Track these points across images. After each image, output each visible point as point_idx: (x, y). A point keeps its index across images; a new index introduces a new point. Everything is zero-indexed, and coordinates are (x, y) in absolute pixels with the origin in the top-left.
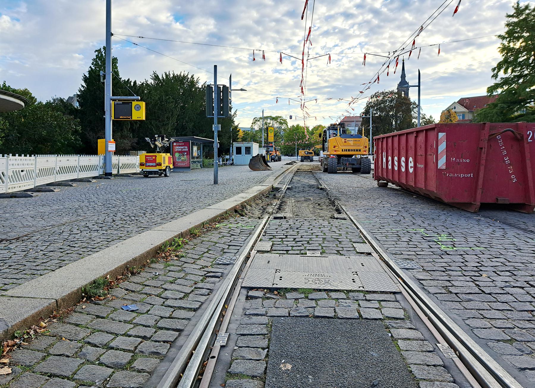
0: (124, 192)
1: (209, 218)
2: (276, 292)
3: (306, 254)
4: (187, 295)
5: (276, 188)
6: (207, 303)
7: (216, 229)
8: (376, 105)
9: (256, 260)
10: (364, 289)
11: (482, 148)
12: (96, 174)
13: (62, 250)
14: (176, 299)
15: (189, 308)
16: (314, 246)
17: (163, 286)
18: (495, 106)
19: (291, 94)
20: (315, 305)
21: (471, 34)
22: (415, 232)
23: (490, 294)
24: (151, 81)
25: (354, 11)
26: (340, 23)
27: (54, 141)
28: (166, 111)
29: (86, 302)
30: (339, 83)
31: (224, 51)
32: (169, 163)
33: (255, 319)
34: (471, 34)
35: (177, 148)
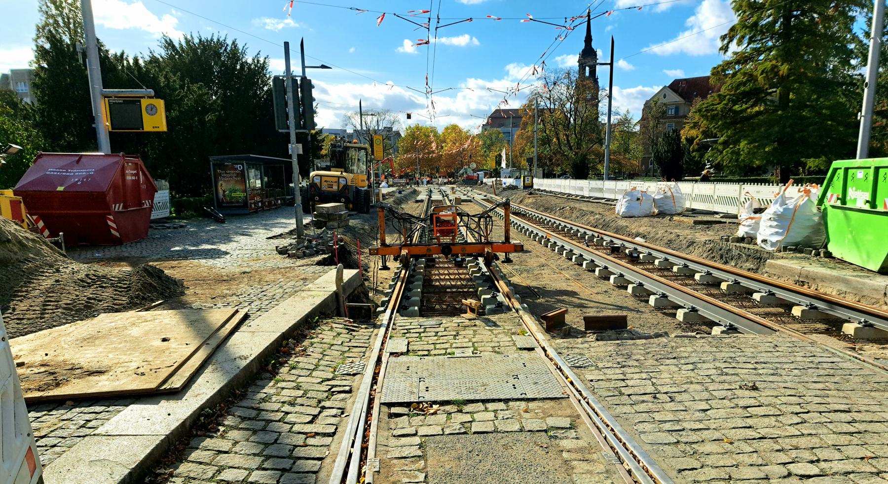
3: (454, 353)
4: (315, 417)
33: (404, 440)
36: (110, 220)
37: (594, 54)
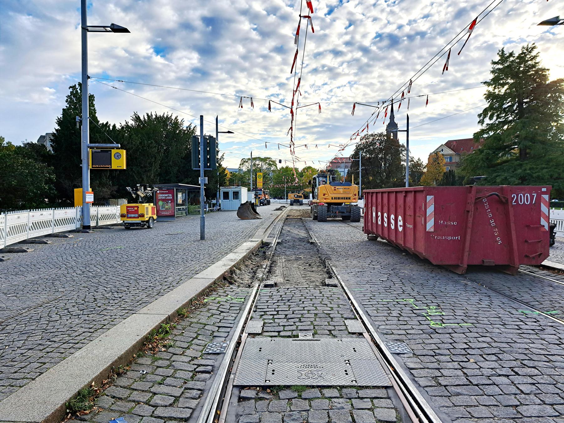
0: (104, 252)
1: (197, 292)
2: (269, 391)
4: (177, 399)
5: (266, 243)
6: (198, 409)
7: (205, 305)
8: (365, 147)
9: (247, 347)
10: (356, 384)
11: (468, 211)
12: (72, 227)
13: (41, 347)
14: (166, 406)
15: (179, 418)
16: (306, 324)
17: (152, 390)
18: (481, 151)
19: (280, 133)
20: (308, 408)
21: (459, 75)
22: (405, 303)
23: (477, 385)
24: (131, 123)
25: (343, 48)
26: (329, 60)
27: (26, 191)
28: (148, 156)
29: (71, 418)
30: (328, 123)
31: (209, 88)
32: (153, 213)
34: (459, 75)
35: (160, 196)
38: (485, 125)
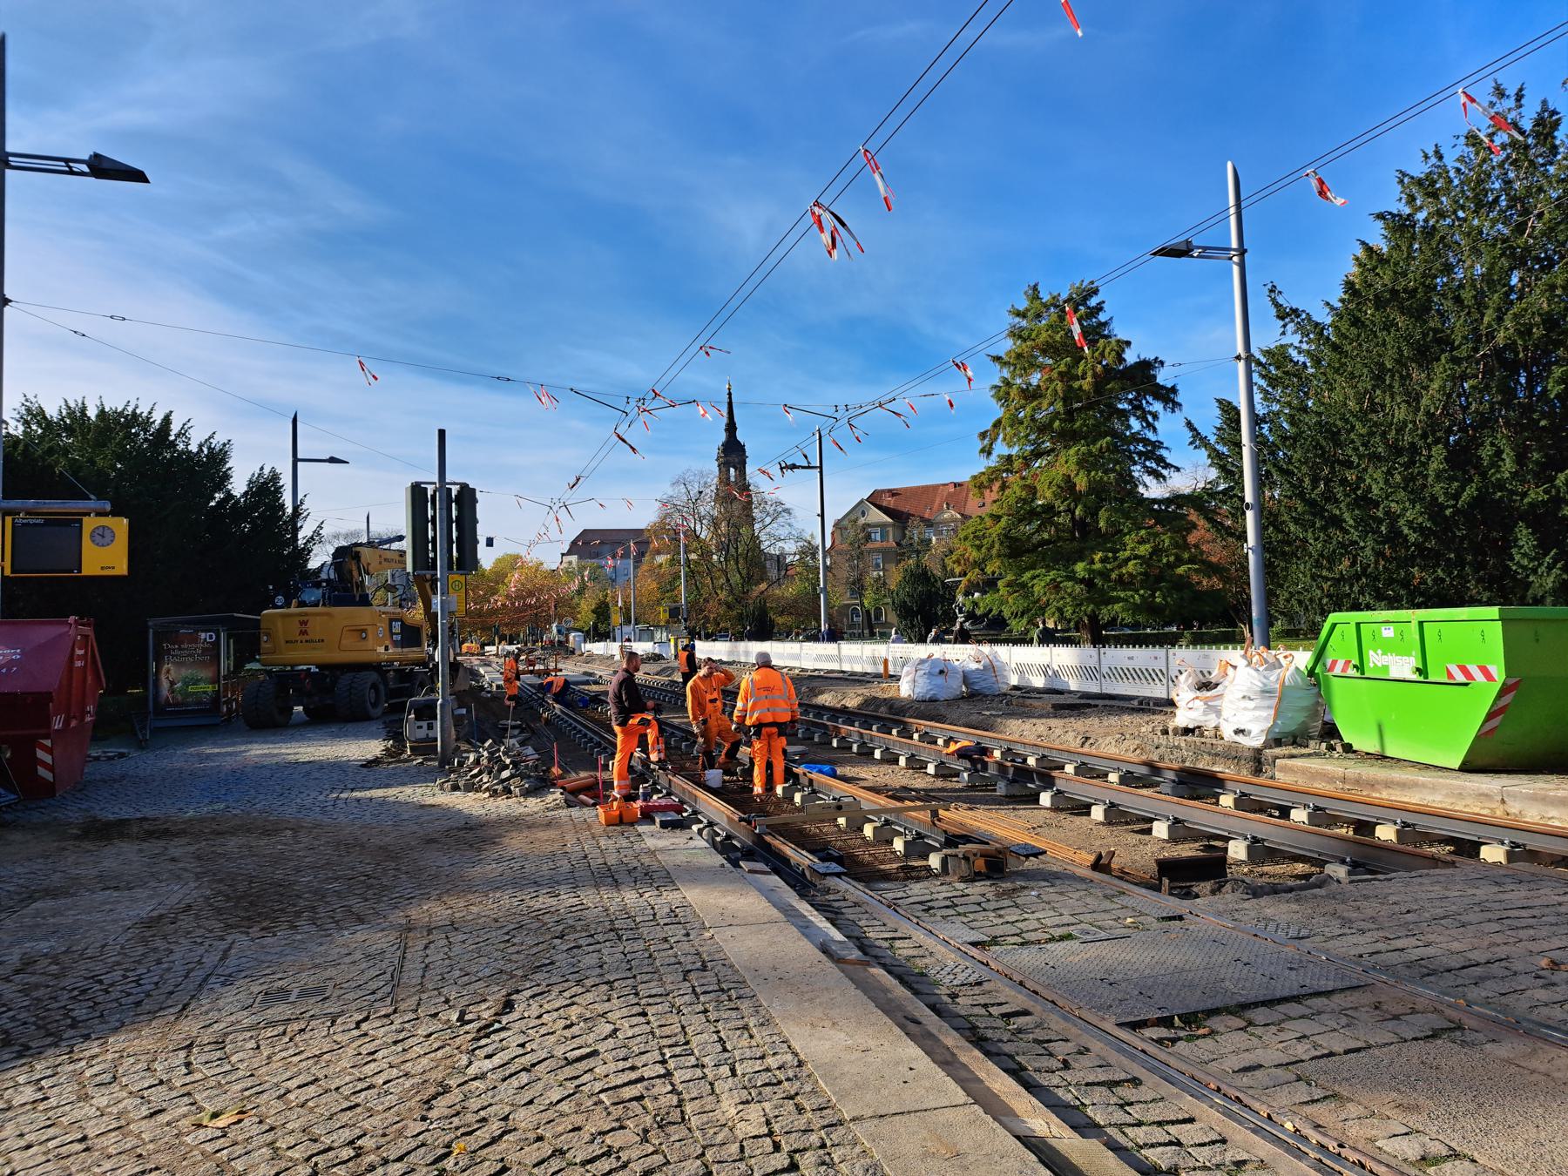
36: (44, 748)
37: (740, 449)
38: (994, 457)
